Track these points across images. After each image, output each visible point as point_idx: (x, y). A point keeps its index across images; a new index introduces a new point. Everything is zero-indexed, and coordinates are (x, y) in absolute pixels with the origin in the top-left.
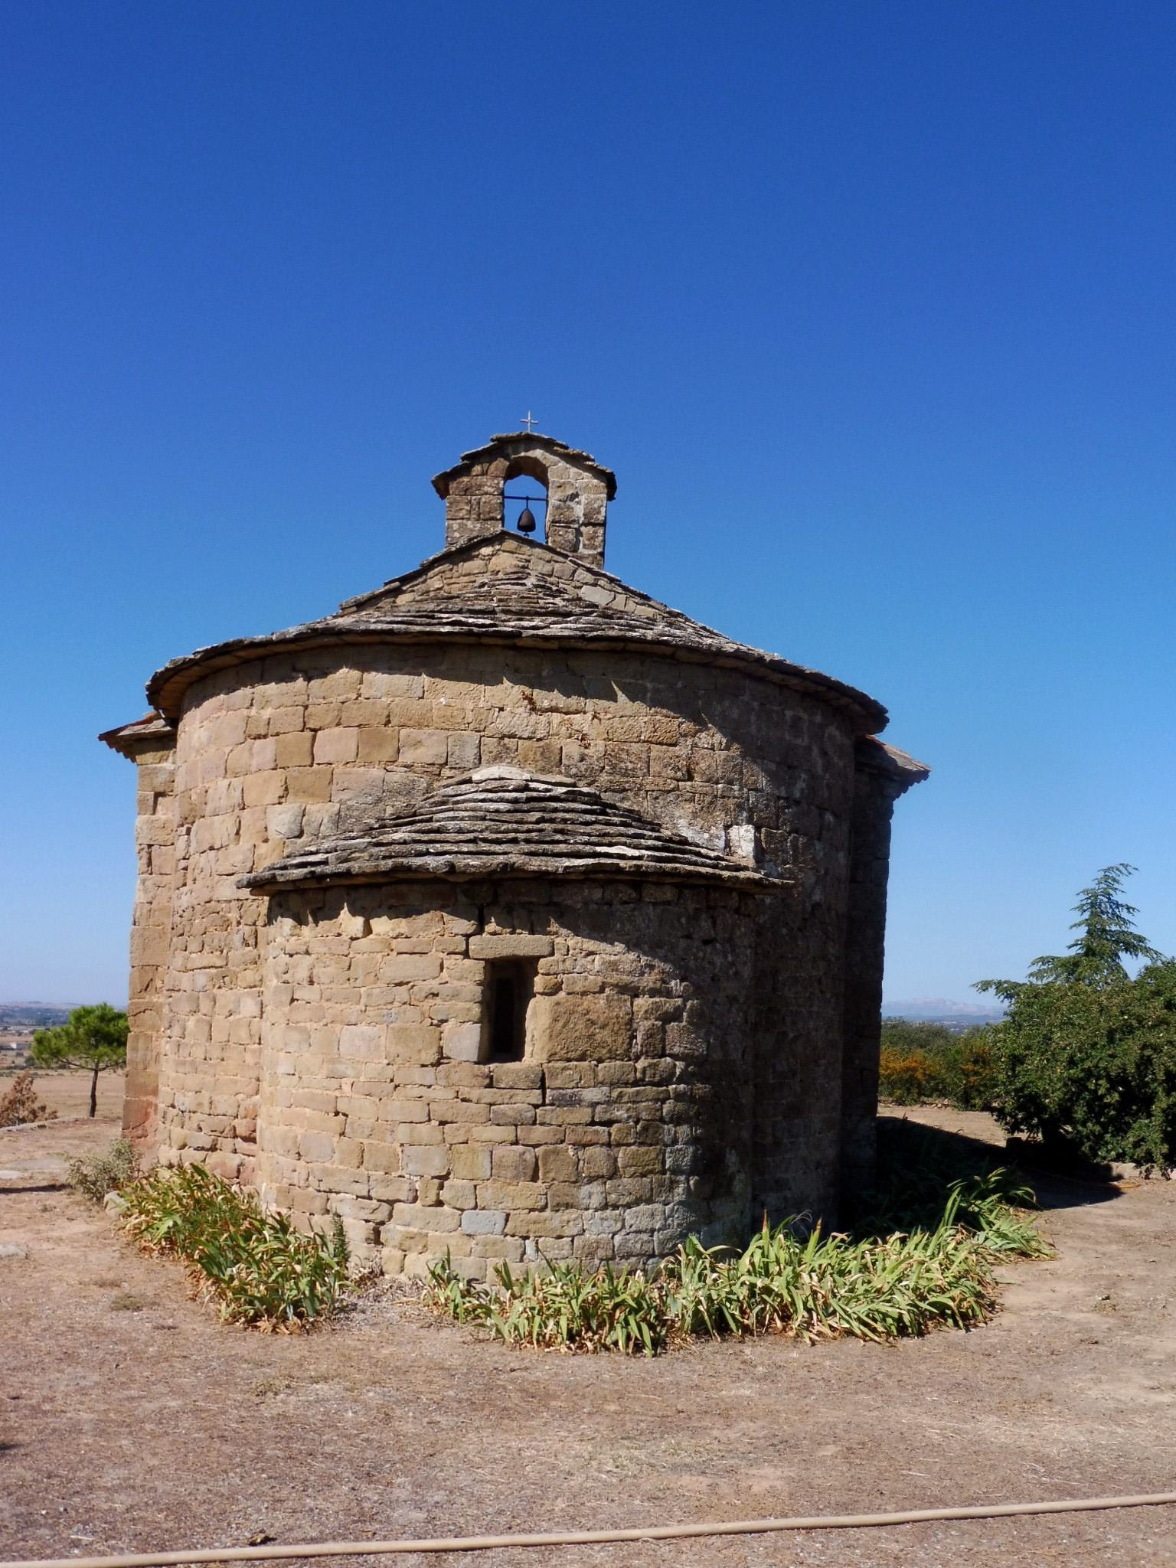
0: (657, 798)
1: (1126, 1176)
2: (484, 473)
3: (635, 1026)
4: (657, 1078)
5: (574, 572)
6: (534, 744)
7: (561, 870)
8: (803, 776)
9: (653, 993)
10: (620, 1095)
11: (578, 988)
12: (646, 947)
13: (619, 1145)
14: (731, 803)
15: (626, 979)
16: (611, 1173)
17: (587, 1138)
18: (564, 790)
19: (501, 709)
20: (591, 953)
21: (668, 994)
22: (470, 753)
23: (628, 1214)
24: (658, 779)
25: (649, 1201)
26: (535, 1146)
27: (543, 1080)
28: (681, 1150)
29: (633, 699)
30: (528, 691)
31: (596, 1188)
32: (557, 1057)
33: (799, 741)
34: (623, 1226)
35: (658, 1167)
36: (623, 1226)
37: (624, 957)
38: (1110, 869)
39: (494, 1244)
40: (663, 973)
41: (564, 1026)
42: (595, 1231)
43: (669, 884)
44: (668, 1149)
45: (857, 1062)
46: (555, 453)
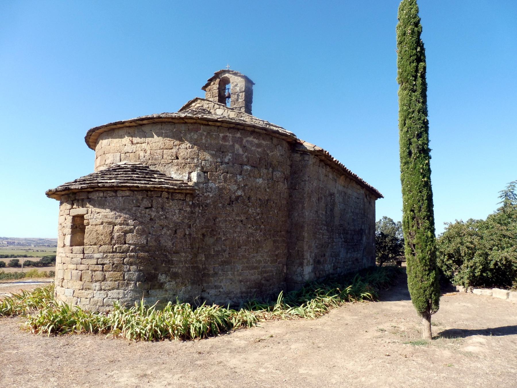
0: (165, 166)
1: (460, 291)
2: (214, 84)
3: (113, 235)
4: (121, 251)
5: (214, 105)
6: (133, 154)
7: (80, 188)
8: (230, 154)
9: (121, 224)
10: (107, 256)
11: (94, 223)
12: (118, 210)
13: (106, 271)
14: (192, 165)
15: (110, 220)
16: (103, 279)
17: (95, 269)
18: (131, 166)
19: (125, 145)
20: (99, 213)
21: (128, 225)
22: (118, 158)
23: (110, 293)
24: (165, 160)
25: (118, 289)
26: (81, 271)
27: (83, 251)
28: (132, 273)
29: (158, 137)
30: (131, 138)
31: (98, 284)
32: (87, 244)
33: (227, 143)
34: (107, 296)
35: (121, 278)
36: (107, 296)
37: (109, 214)
38: (511, 183)
39: (71, 299)
40: (125, 218)
41: (89, 235)
42: (97, 297)
44: (126, 273)
45: (296, 248)
46: (231, 74)
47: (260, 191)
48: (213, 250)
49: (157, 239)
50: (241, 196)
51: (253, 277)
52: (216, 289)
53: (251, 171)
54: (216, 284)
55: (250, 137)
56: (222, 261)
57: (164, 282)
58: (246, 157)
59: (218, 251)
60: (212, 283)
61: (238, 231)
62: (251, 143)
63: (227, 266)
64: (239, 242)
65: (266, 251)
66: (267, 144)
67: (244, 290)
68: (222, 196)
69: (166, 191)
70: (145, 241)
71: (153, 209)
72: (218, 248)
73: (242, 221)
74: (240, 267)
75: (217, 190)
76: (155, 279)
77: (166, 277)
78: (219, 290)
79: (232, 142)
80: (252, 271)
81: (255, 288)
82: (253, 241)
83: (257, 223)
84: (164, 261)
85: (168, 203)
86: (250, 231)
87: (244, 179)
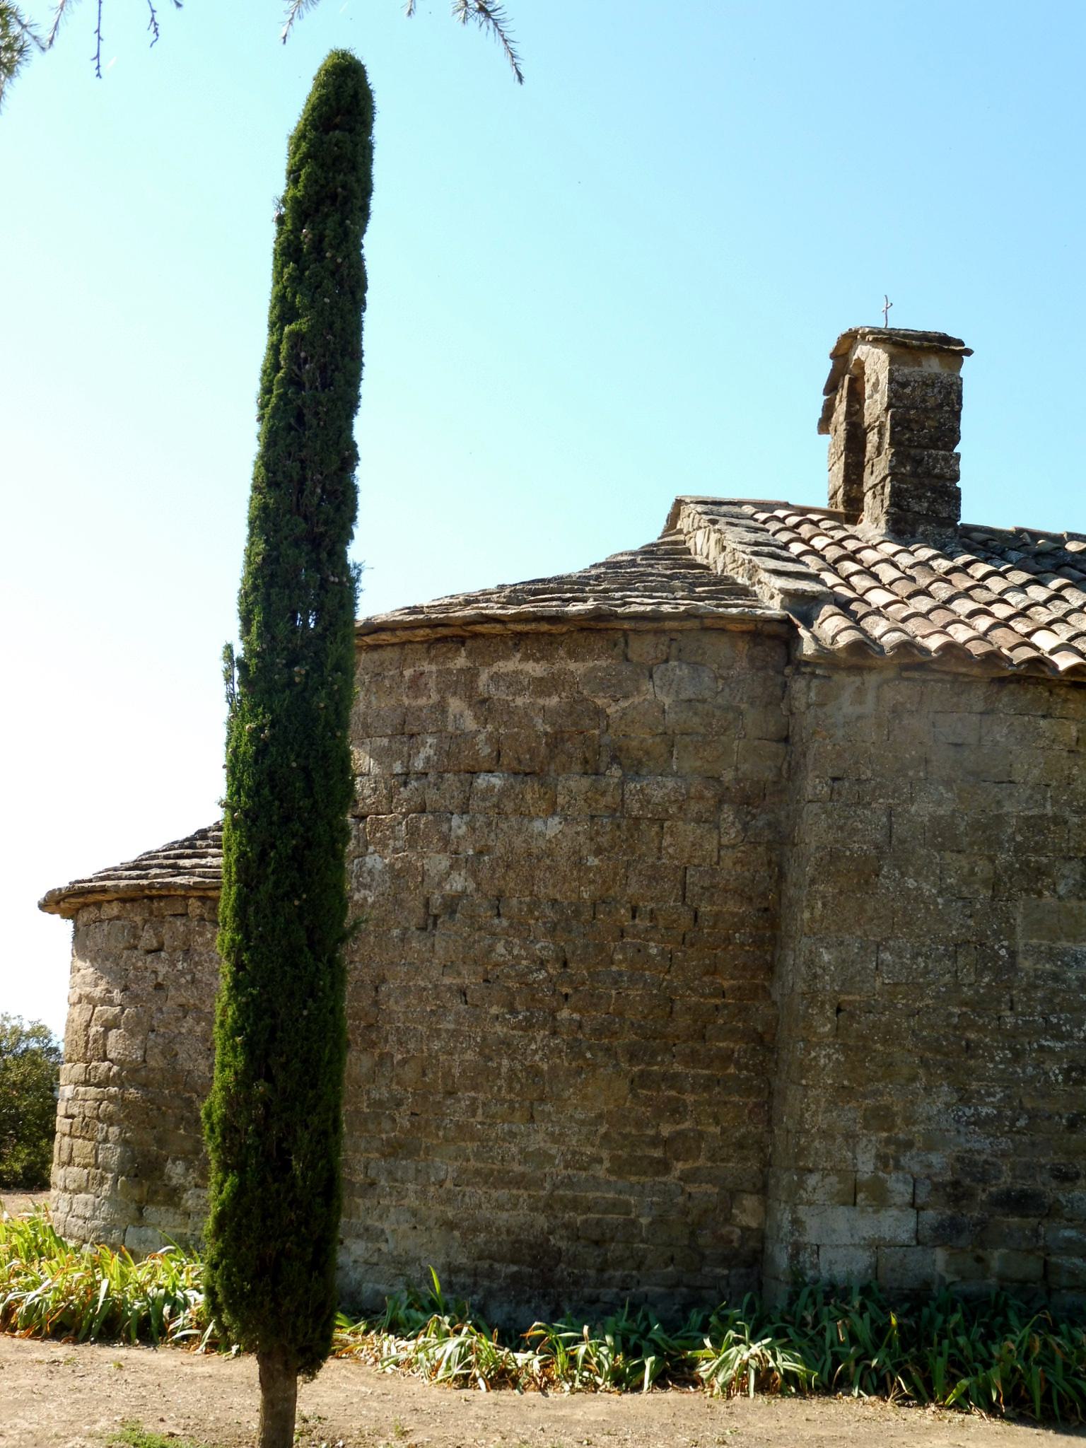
25: (86, 1190)
33: (422, 701)
35: (92, 1161)
43: (195, 897)
47: (549, 868)
48: (365, 1097)
49: (169, 1053)
50: (463, 894)
51: (505, 1215)
52: (368, 1240)
53: (504, 792)
54: (369, 1222)
55: (506, 658)
56: (389, 1142)
57: (181, 1185)
58: (489, 738)
59: (380, 1103)
60: (359, 1218)
61: (447, 1031)
62: (513, 682)
63: (404, 1162)
64: (448, 1074)
65: (579, 1116)
66: (594, 668)
67: (462, 1260)
68: (402, 900)
69: (195, 897)
70: (140, 1053)
71: (163, 954)
72: (381, 1092)
73: (463, 992)
74: (445, 1168)
75: (387, 877)
76: (158, 1174)
77: (187, 1170)
78: (379, 1245)
79: (439, 691)
80: (502, 1194)
81: (514, 1262)
82: (511, 1070)
83: (533, 999)
84: (182, 1119)
85: (201, 934)
86: (500, 1029)
87: (474, 829)
